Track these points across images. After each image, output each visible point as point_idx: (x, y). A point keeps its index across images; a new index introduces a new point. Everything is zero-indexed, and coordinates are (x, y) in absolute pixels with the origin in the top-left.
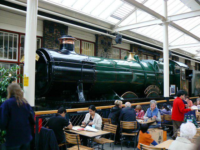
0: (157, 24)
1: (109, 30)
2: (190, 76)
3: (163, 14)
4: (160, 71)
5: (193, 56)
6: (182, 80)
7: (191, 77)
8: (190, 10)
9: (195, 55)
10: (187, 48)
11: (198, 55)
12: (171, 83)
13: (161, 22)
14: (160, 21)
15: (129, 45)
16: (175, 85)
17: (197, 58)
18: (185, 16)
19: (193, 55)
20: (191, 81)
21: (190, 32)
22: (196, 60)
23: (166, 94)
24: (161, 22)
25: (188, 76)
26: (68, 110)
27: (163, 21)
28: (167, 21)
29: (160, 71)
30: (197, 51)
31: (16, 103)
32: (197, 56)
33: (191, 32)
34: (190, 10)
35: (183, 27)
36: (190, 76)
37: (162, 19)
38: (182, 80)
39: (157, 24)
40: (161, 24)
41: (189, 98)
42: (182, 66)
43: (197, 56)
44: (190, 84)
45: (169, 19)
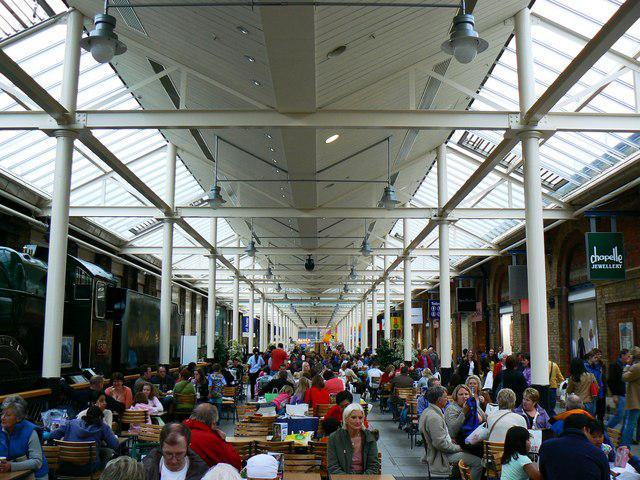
0: (37, 129)
1: (116, 248)
2: (117, 306)
3: (59, 94)
4: (31, 287)
5: (122, 244)
6: (95, 320)
7: (121, 311)
8: (133, 105)
9: (127, 242)
10: (105, 219)
11: (136, 244)
12: (67, 330)
13: (162, 215)
14: (51, 122)
15: (122, 268)
16: (72, 338)
17: (130, 252)
18: (118, 120)
19: (120, 240)
20: (121, 323)
21: (36, 80)
22: (126, 257)
23: (51, 368)
24: (162, 215)
25: (112, 308)
26: (472, 364)
27: (59, 121)
28: (76, 126)
29: (31, 287)
30: (132, 231)
31: (621, 371)
32: (132, 247)
33: (131, 168)
34: (133, 105)
35: (112, 149)
36: (117, 306)
37: (57, 115)
38: (95, 320)
39: (37, 129)
40: (50, 133)
41: (123, 380)
42: (97, 276)
43: (132, 247)
44: (117, 332)
45: (81, 122)
